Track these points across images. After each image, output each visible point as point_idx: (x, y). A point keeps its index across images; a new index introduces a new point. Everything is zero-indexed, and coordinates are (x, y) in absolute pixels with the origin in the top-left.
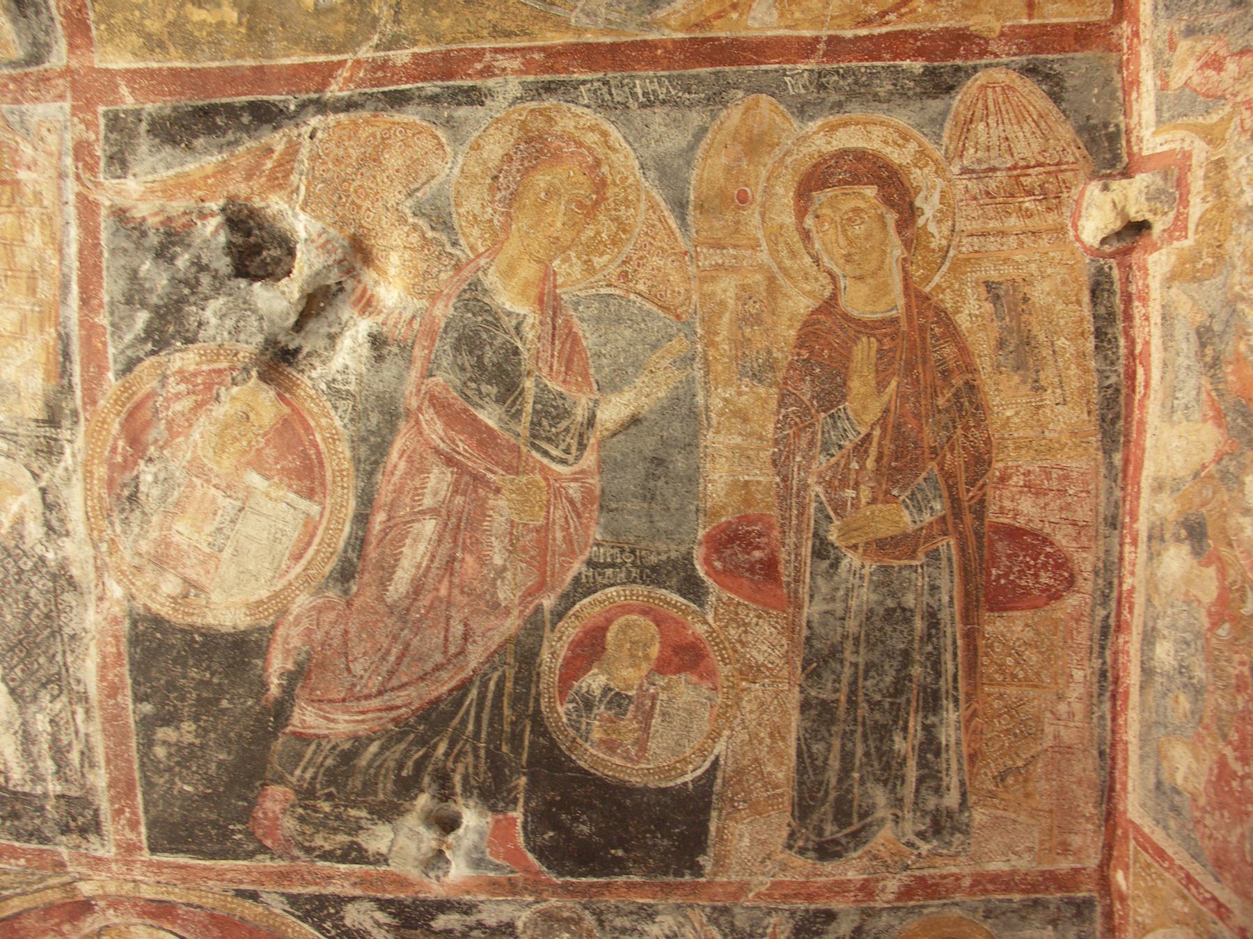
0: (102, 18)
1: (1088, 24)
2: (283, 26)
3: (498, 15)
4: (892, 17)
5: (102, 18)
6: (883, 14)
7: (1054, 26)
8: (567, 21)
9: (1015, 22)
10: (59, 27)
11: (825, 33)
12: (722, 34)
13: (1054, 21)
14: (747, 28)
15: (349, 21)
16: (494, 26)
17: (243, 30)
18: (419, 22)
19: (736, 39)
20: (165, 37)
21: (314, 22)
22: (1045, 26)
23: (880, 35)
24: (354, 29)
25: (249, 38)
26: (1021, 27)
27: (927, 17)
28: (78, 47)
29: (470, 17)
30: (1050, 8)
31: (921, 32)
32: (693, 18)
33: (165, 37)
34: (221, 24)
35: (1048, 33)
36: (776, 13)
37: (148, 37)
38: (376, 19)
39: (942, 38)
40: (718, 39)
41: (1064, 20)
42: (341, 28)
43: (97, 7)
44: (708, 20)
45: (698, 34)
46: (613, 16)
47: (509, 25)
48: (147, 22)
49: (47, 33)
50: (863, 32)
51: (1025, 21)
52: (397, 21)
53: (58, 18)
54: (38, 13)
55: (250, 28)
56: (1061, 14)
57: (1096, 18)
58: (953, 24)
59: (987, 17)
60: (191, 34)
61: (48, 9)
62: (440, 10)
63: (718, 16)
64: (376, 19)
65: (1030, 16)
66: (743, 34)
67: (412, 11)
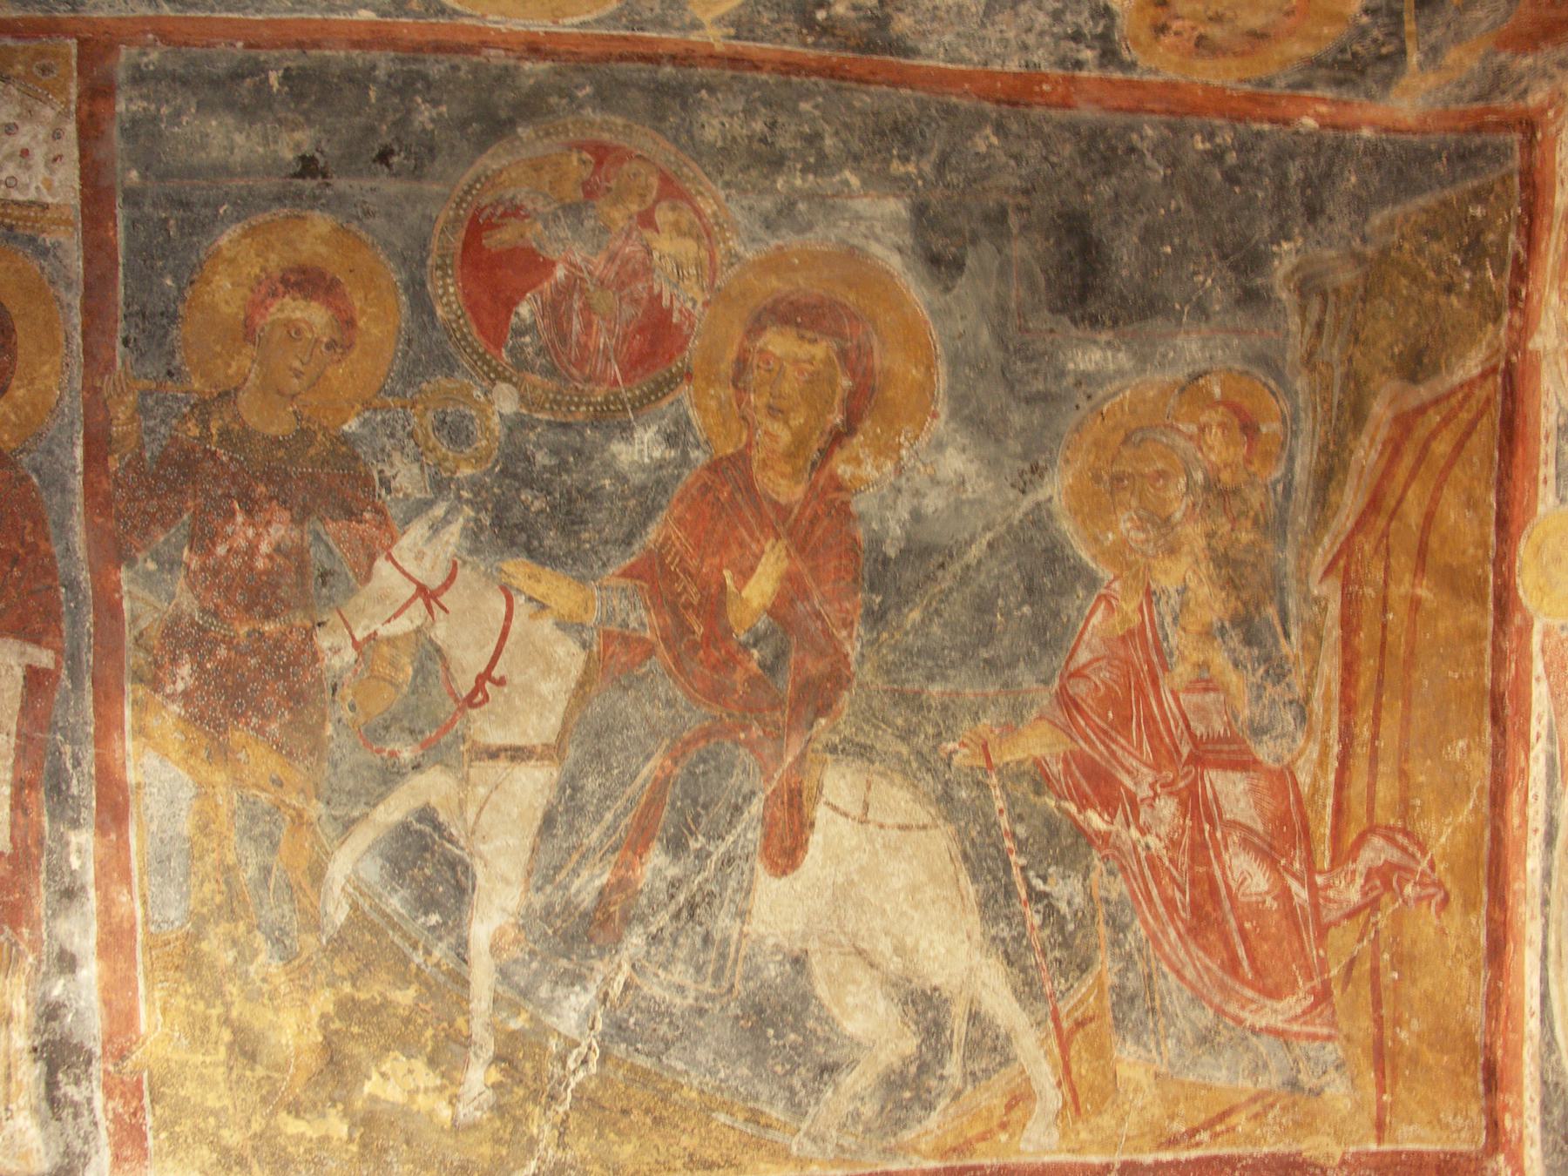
0: (163, 1125)
1: (1453, 1154)
2: (408, 1142)
3: (696, 1141)
4: (1204, 1136)
5: (163, 1125)
6: (1193, 1132)
7: (1410, 1154)
8: (787, 1149)
9: (1362, 1148)
10: (103, 1133)
11: (1117, 1159)
12: (986, 1162)
13: (1410, 1147)
14: (1019, 1152)
15: (498, 1141)
16: (691, 1156)
17: (354, 1148)
18: (591, 1148)
19: (1004, 1167)
20: (248, 1152)
21: (450, 1142)
22: (1400, 1153)
23: (1188, 1162)
24: (504, 1152)
25: (362, 1157)
26: (1367, 1154)
27: (1250, 1139)
28: (126, 1159)
29: (659, 1142)
30: (1404, 1130)
31: (1240, 1159)
32: (950, 1141)
33: (248, 1152)
34: (325, 1140)
35: (1403, 1164)
36: (1056, 1134)
37: (226, 1151)
38: (533, 1142)
39: (1267, 1167)
40: (981, 1168)
41: (1424, 1147)
42: (486, 1149)
43: (158, 1111)
44: (969, 1142)
45: (955, 1162)
46: (848, 1141)
47: (711, 1154)
48: (225, 1133)
49: (86, 1141)
50: (1167, 1156)
51: (1373, 1147)
52: (562, 1145)
53: (104, 1123)
54: (76, 1116)
55: (364, 1146)
56: (1419, 1139)
57: (1463, 1147)
58: (1282, 1148)
59: (1325, 1140)
60: (284, 1149)
61: (91, 1111)
62: (619, 1133)
63: (983, 1137)
64: (533, 1142)
65: (1380, 1140)
66: (1013, 1160)
67: (582, 1132)
